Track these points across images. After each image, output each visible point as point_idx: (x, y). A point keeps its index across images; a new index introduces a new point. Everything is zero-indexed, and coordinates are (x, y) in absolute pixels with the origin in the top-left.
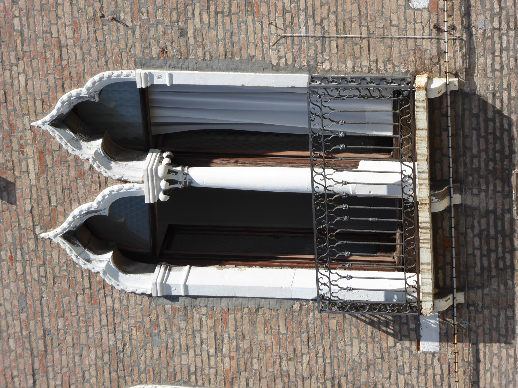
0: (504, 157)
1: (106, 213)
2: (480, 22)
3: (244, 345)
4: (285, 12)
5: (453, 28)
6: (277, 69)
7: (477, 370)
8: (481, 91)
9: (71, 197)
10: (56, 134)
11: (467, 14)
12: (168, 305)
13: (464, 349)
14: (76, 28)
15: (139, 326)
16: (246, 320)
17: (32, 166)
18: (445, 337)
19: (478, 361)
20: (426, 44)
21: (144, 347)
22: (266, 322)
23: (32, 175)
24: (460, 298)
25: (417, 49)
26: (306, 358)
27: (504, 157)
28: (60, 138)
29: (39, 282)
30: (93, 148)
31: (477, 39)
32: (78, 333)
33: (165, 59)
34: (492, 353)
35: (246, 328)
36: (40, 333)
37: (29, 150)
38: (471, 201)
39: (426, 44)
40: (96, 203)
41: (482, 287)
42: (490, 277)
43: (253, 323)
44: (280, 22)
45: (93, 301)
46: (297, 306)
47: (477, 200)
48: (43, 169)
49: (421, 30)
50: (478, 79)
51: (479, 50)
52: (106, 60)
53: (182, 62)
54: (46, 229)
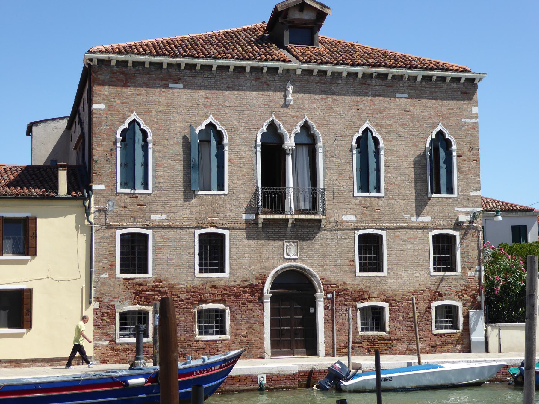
0: (302, 238)
1: (312, 132)
2: (339, 233)
3: (242, 165)
4: (340, 183)
5: (337, 226)
6: (324, 180)
7: (237, 229)
8: (320, 233)
9: (285, 123)
10: (303, 121)
11: (341, 230)
12: (253, 146)
13: (244, 226)
14: (332, 129)
15: (246, 137)
16: (249, 167)
17: (293, 113)
18: (247, 221)
19: (240, 230)
20: (333, 219)
21: (239, 138)
22: (249, 172)
23: (290, 113)
24: (260, 225)
25: (331, 217)
26: (239, 182)
27: (302, 238)
28: (302, 122)
29: (258, 111)
30: (298, 129)
31: (334, 232)
32: (243, 120)
33: (325, 152)
34: (243, 234)
35: (247, 167)
36: (243, 109)
37: (297, 113)
38: (288, 229)
39: (333, 219)
40: (283, 129)
41: (263, 231)
42: (266, 234)
43: (249, 168)
44: (337, 182)
45: (253, 125)
46: (255, 181)
47: (289, 231)
48: (293, 116)
49: (336, 218)
50: (324, 232)
51: (331, 232)
52: (324, 136)
53: (325, 156)
54: (275, 115)
